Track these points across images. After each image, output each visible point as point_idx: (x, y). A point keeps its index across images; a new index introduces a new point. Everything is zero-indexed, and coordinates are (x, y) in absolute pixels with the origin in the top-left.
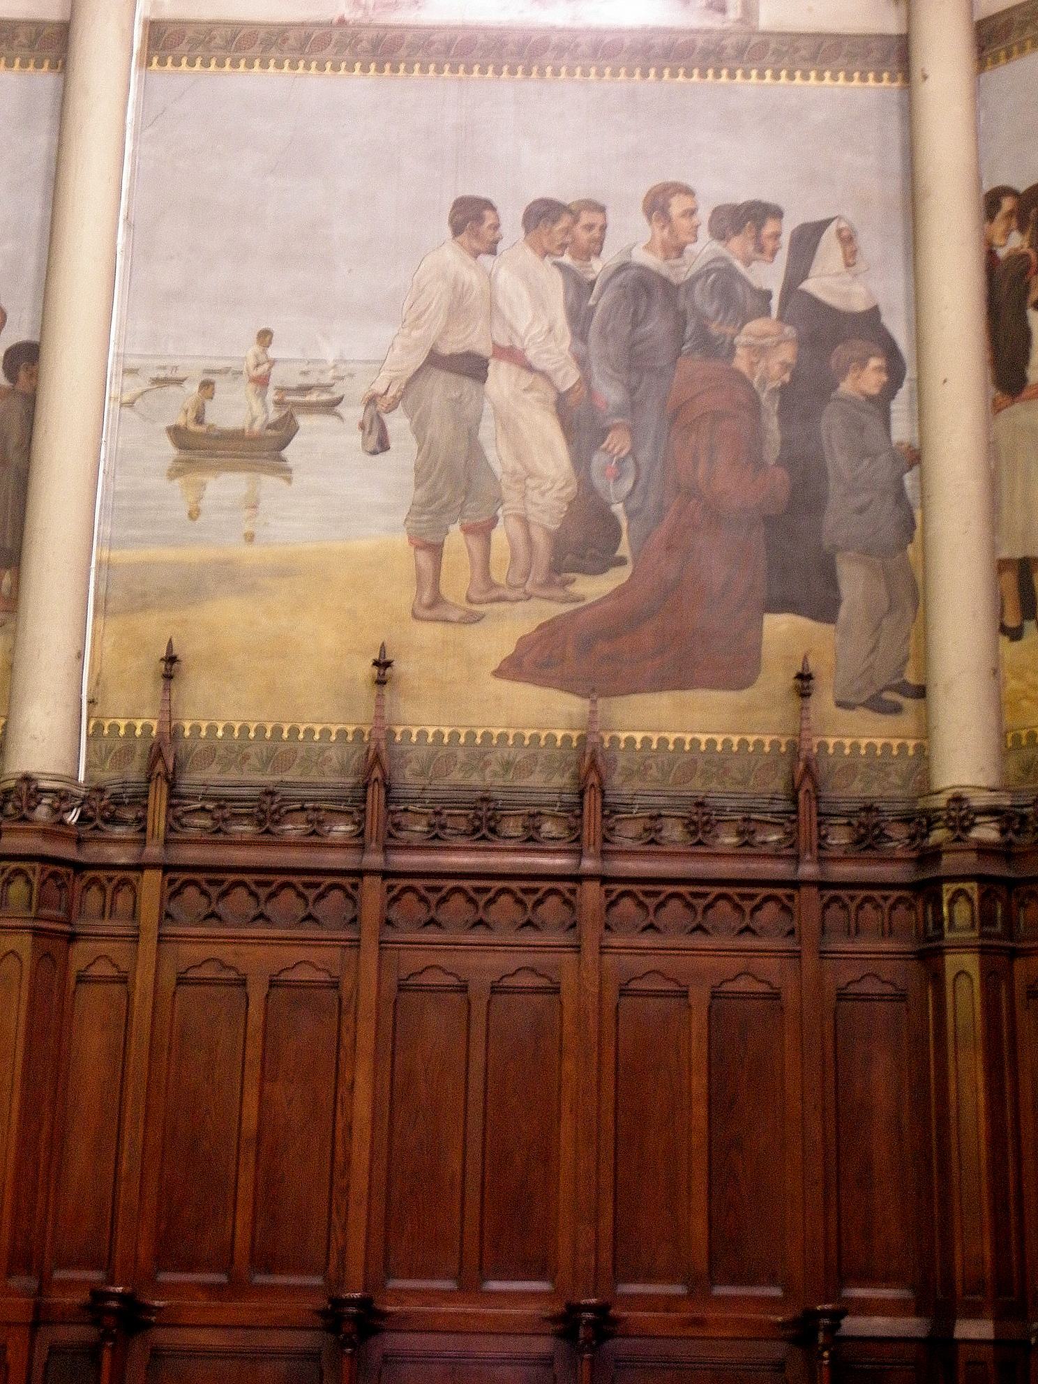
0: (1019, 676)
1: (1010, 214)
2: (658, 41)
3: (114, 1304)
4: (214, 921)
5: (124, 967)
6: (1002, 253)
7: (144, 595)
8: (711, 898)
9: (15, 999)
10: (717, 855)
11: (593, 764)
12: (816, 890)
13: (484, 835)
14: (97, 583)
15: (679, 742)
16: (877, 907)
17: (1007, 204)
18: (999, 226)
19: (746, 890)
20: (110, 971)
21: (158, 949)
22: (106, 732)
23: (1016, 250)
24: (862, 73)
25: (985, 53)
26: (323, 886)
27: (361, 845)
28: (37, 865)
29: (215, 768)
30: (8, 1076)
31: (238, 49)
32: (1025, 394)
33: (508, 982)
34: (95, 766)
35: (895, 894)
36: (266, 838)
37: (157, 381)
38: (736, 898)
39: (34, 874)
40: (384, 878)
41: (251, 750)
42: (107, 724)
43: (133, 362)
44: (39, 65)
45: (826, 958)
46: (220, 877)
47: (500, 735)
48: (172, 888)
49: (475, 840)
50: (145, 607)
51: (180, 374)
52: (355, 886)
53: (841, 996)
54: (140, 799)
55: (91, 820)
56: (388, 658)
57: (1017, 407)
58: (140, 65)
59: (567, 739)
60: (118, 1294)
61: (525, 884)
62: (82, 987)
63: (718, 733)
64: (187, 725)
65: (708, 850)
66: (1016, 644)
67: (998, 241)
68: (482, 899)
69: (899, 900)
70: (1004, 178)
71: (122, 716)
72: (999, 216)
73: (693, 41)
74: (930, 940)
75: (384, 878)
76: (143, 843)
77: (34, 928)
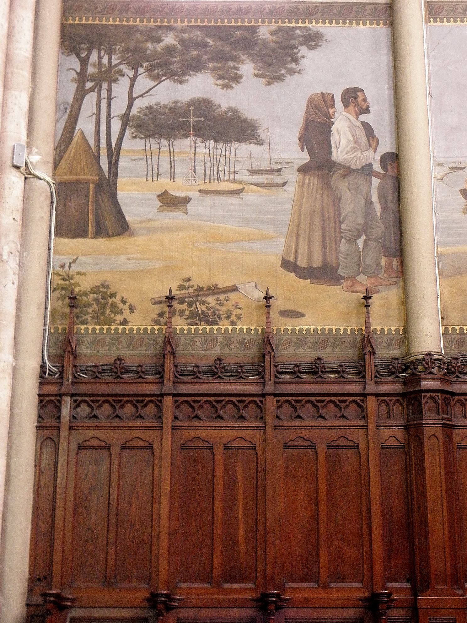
2: (234, 6)
3: (52, 599)
4: (219, 420)
7: (459, 268)
9: (437, 456)
10: (125, 383)
12: (171, 397)
14: (438, 263)
15: (308, 330)
19: (220, 398)
20: (395, 443)
22: (450, 332)
24: (269, 19)
26: (202, 401)
28: (439, 394)
30: (439, 493)
31: (108, 13)
34: (447, 347)
35: (395, 398)
36: (341, 380)
37: (452, 168)
39: (439, 399)
40: (275, 397)
42: (450, 328)
43: (441, 160)
44: (378, 24)
46: (220, 398)
47: (329, 329)
49: (216, 378)
50: (460, 273)
51: (462, 165)
55: (453, 373)
56: (271, 295)
58: (426, 23)
59: (256, 330)
60: (165, 594)
69: (397, 401)
71: (457, 324)
73: (216, 6)
75: (173, 397)
76: (264, 384)
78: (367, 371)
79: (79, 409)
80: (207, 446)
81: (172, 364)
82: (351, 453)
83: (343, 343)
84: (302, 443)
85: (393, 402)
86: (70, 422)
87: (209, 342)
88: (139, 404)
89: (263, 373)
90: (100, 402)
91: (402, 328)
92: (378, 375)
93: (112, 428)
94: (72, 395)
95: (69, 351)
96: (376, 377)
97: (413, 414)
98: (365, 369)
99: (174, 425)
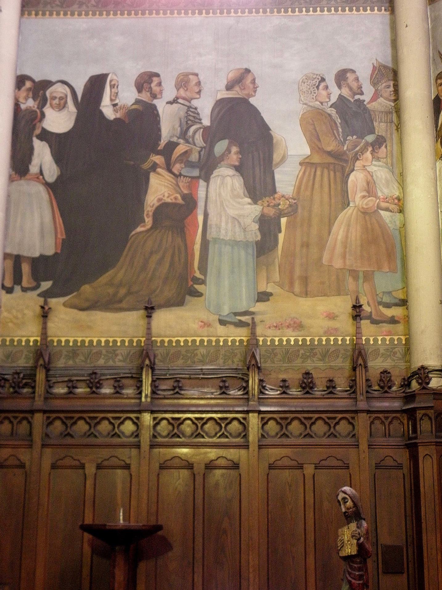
0: (9, 311)
1: (29, 90)
5: (128, 462)
6: (23, 107)
8: (338, 419)
10: (316, 398)
11: (360, 353)
13: (308, 391)
16: (383, 423)
17: (28, 84)
18: (22, 94)
19: (92, 415)
21: (41, 451)
23: (30, 107)
25: (24, 9)
27: (247, 398)
29: (299, 360)
32: (28, 177)
33: (106, 463)
38: (303, 419)
41: (118, 352)
45: (371, 448)
46: (95, 415)
48: (49, 421)
52: (353, 418)
53: (271, 467)
54: (32, 376)
57: (22, 182)
61: (306, 415)
62: (165, 472)
63: (181, 337)
64: (261, 339)
65: (311, 396)
66: (9, 296)
67: (21, 100)
68: (93, 423)
70: (27, 71)
72: (23, 88)
74: (410, 439)
77: (437, 442)
78: (358, 386)
79: (51, 428)
80: (343, 466)
81: (364, 378)
82: (185, 473)
83: (315, 354)
84: (335, 463)
85: (389, 420)
86: (150, 441)
87: (92, 355)
88: (330, 420)
89: (355, 387)
90: (122, 419)
91: (144, 339)
92: (369, 391)
93: (289, 447)
94: (45, 412)
95: (41, 365)
96: (367, 392)
97: (412, 433)
98: (356, 384)
99: (371, 444)
